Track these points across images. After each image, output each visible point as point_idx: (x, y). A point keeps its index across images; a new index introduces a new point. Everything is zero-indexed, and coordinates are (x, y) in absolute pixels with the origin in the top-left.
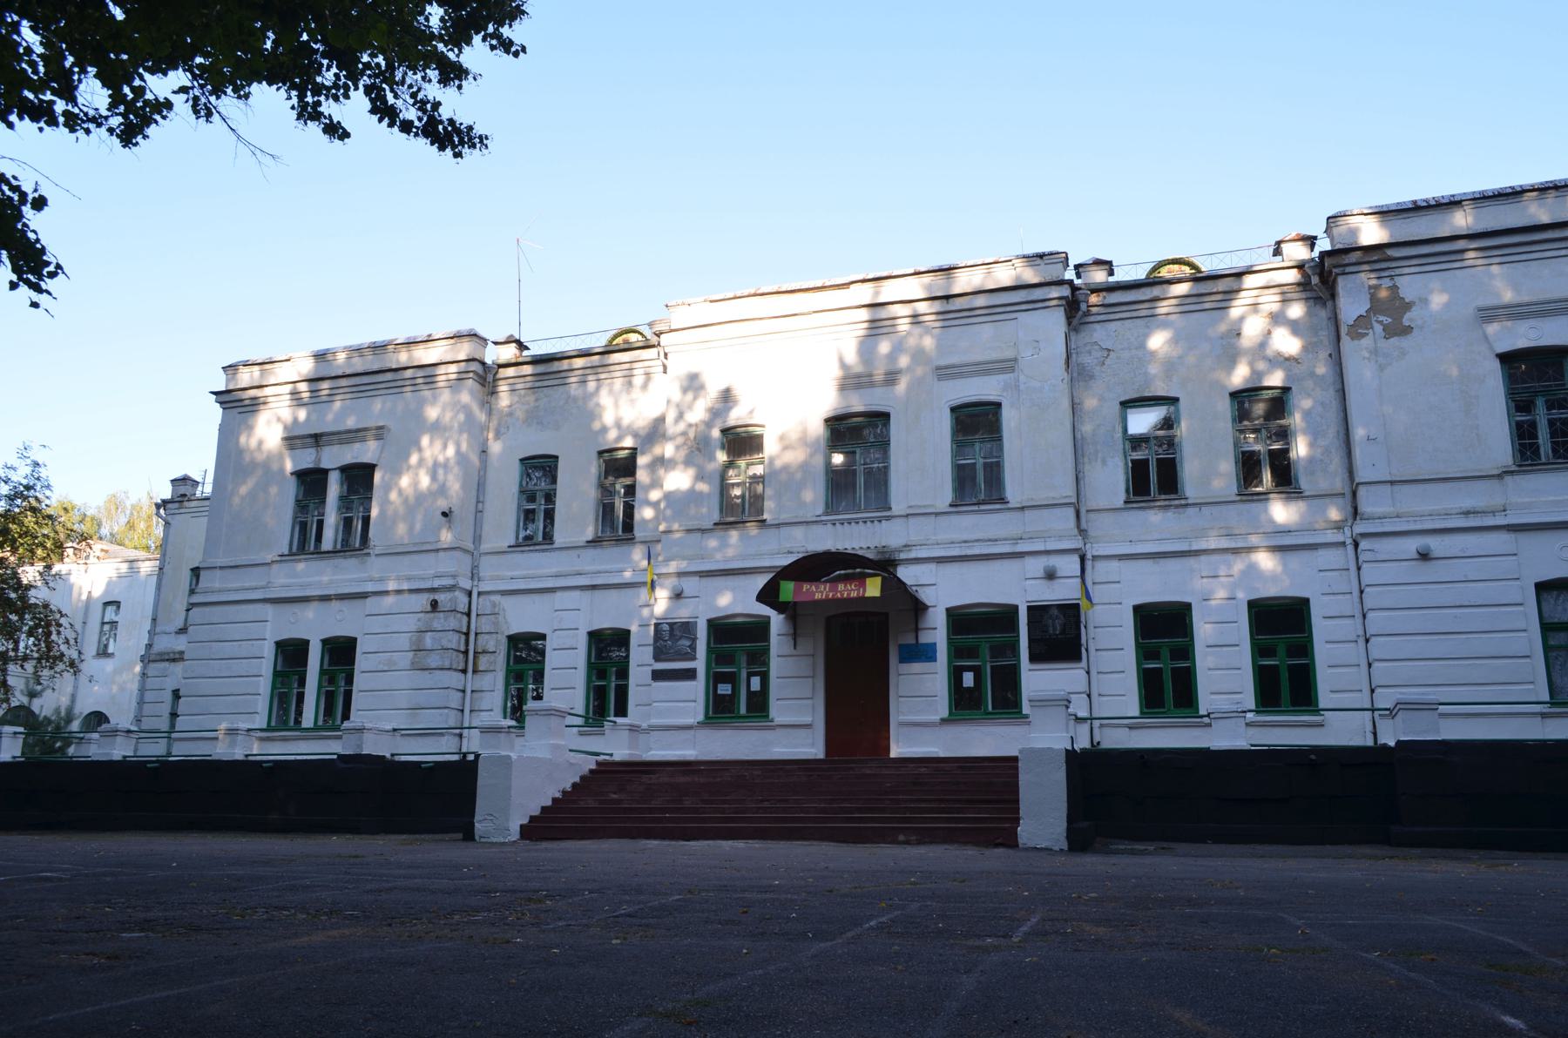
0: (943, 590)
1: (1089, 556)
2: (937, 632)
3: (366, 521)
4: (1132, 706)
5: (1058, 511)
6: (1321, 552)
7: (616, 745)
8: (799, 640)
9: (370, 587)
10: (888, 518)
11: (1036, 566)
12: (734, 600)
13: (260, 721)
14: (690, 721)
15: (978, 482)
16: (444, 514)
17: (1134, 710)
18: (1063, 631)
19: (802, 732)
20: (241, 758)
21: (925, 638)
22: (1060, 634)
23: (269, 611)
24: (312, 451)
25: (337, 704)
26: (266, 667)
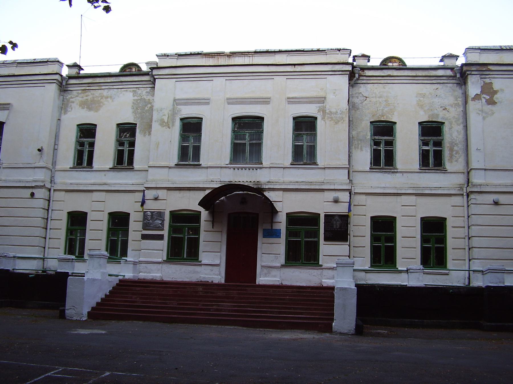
0: (286, 205)
2: (281, 223)
5: (341, 170)
6: (453, 198)
8: (215, 224)
10: (261, 168)
11: (331, 195)
12: (191, 202)
14: (160, 260)
15: (304, 153)
16: (39, 150)
18: (340, 228)
21: (276, 227)
22: (338, 228)
25: (434, 253)
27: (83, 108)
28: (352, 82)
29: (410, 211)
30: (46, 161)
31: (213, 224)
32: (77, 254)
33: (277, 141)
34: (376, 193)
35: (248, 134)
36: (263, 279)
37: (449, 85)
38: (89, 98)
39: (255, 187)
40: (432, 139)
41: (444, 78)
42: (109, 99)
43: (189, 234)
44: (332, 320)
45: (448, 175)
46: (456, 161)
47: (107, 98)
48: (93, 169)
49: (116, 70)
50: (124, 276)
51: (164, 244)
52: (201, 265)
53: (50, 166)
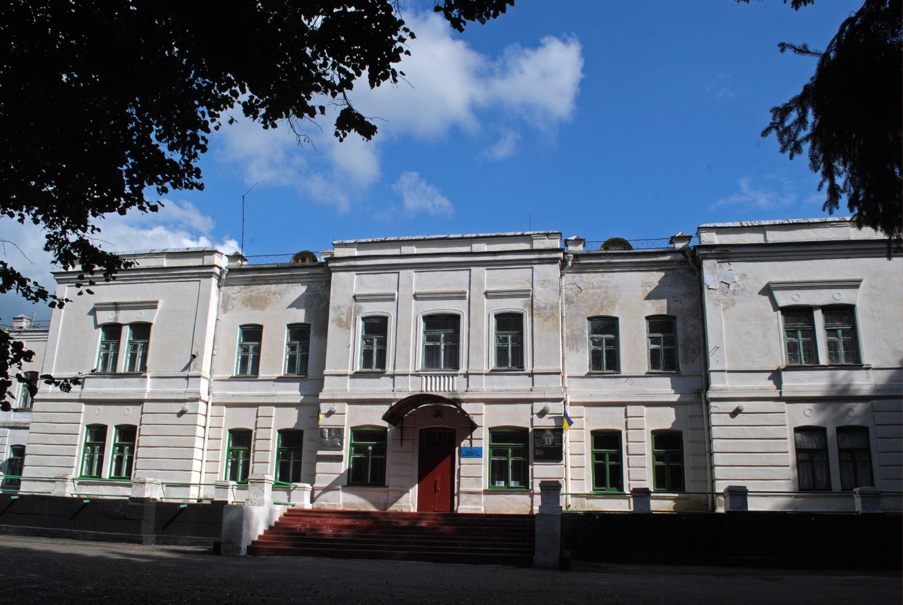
0: (486, 419)
2: (482, 439)
4: (588, 486)
7: (302, 498)
9: (884, 403)
11: (538, 407)
12: (375, 417)
15: (511, 357)
18: (553, 444)
20: (70, 496)
24: (113, 312)
27: (247, 306)
28: (564, 271)
32: (240, 480)
33: (479, 342)
36: (465, 506)
38: (254, 294)
39: (451, 397)
42: (277, 295)
44: (533, 553)
46: (693, 361)
47: (275, 293)
49: (288, 260)
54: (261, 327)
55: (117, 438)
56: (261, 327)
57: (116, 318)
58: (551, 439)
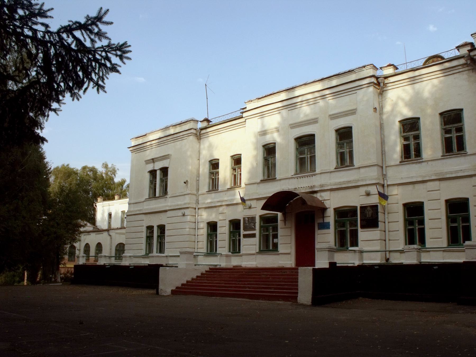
0: (333, 202)
1: (386, 185)
2: (330, 218)
3: (218, 178)
8: (286, 222)
10: (315, 175)
11: (362, 191)
13: (143, 253)
14: (254, 252)
15: (345, 159)
16: (185, 183)
17: (445, 244)
18: (372, 216)
19: (287, 256)
21: (326, 220)
22: (370, 217)
23: (143, 217)
24: (152, 164)
26: (144, 235)
29: (434, 195)
30: (191, 189)
31: (285, 222)
33: (326, 149)
34: (405, 184)
35: (306, 149)
37: (465, 73)
40: (453, 127)
41: (460, 67)
43: (350, 227)
45: (468, 157)
48: (423, 160)
50: (354, 263)
51: (256, 241)
52: (278, 254)
53: (195, 192)
54: (351, 128)
55: (336, 217)
56: (351, 128)
57: (154, 167)
58: (370, 213)
